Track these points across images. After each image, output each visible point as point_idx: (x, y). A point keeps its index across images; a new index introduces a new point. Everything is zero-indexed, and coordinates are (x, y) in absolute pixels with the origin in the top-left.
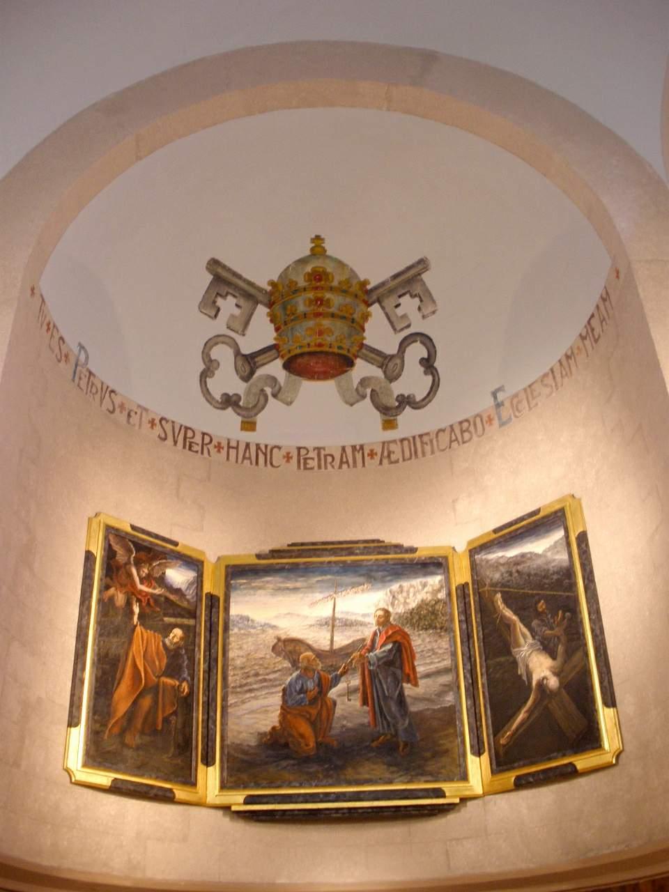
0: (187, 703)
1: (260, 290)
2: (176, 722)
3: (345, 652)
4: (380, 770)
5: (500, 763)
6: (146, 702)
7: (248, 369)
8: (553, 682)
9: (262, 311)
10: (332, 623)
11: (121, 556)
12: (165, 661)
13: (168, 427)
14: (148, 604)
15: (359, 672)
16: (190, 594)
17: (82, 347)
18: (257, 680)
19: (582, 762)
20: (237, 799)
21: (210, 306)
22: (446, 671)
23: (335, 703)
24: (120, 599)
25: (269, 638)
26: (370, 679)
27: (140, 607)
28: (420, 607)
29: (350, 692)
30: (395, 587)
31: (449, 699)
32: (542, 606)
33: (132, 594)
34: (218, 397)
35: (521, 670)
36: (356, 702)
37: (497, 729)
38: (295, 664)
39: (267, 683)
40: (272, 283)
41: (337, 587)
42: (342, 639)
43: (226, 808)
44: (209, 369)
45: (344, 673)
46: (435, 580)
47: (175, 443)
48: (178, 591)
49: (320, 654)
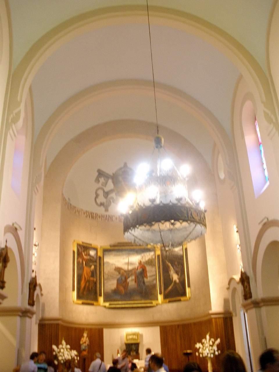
0: (95, 283)
1: (110, 175)
2: (93, 288)
3: (131, 271)
4: (138, 298)
5: (165, 297)
6: (88, 284)
7: (106, 195)
8: (178, 281)
9: (110, 181)
10: (128, 264)
11: (80, 250)
12: (91, 274)
13: (88, 214)
14: (87, 261)
15: (134, 275)
16: (95, 257)
17: (69, 199)
18: (110, 277)
19: (182, 298)
20: (107, 304)
21: (97, 180)
22: (154, 275)
23: (129, 283)
24: (81, 261)
25: (114, 267)
26: (137, 278)
27: (85, 261)
28: (148, 260)
29: (132, 280)
30: (143, 255)
31: (155, 282)
32: (176, 263)
33: (83, 259)
34: (99, 204)
35: (171, 277)
36: (133, 283)
37: (165, 288)
38: (119, 273)
39: (113, 278)
40: (113, 174)
41: (129, 255)
42: (130, 268)
43: (105, 307)
44: (97, 196)
45: (131, 275)
46: (152, 253)
47: (89, 217)
48: (93, 257)
49: (125, 271)
